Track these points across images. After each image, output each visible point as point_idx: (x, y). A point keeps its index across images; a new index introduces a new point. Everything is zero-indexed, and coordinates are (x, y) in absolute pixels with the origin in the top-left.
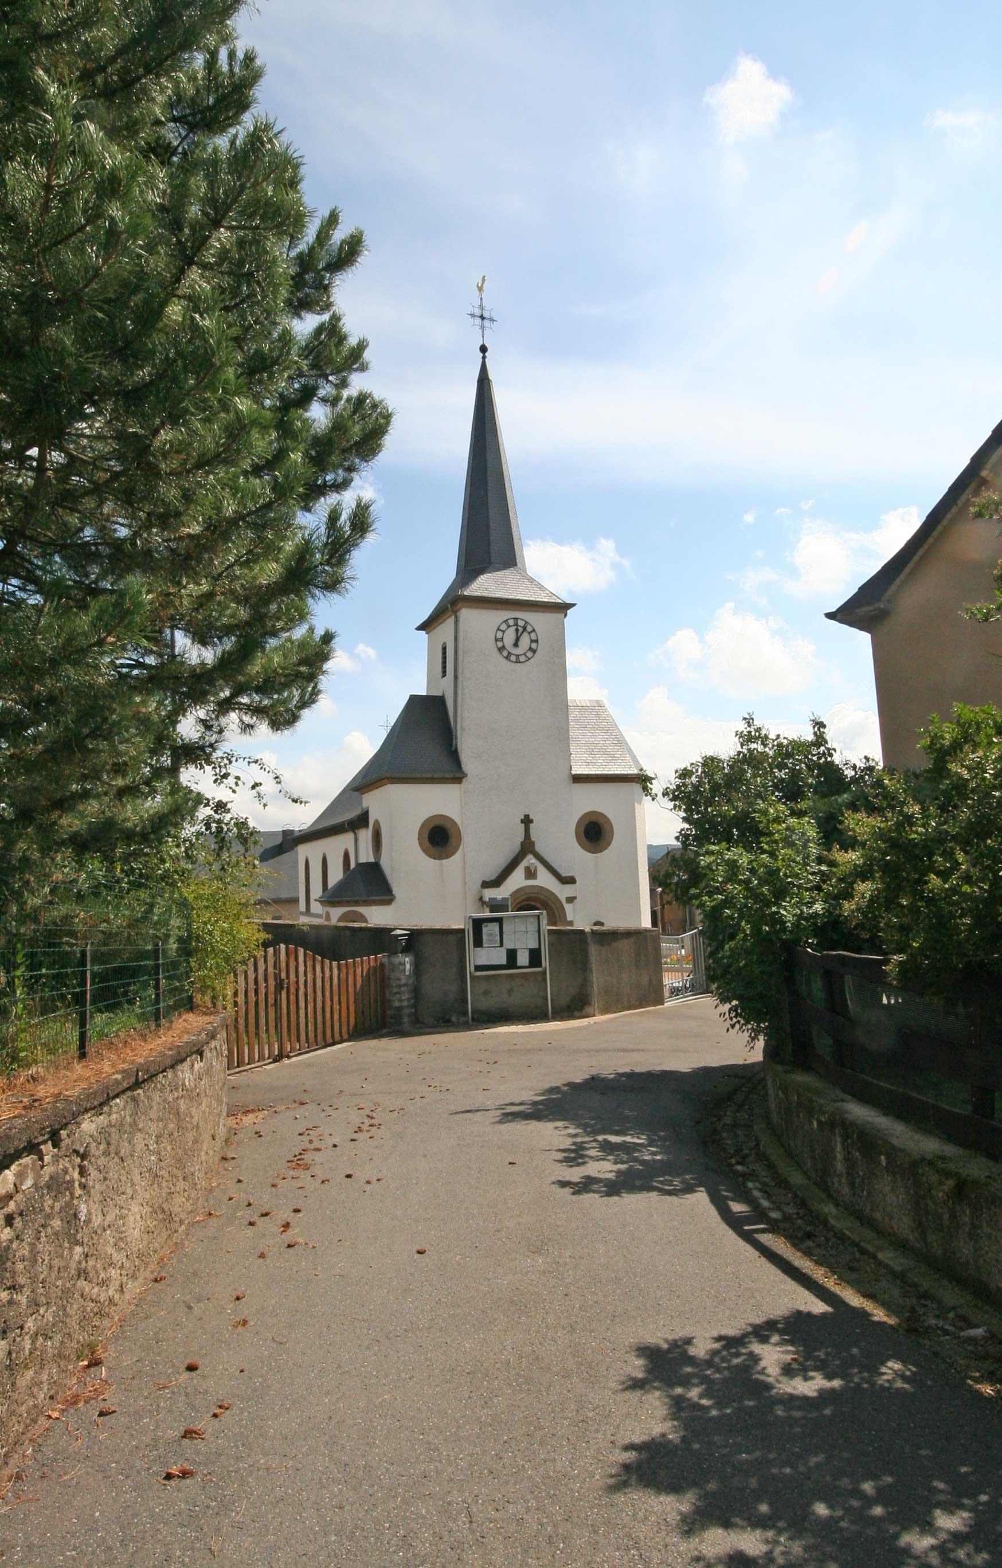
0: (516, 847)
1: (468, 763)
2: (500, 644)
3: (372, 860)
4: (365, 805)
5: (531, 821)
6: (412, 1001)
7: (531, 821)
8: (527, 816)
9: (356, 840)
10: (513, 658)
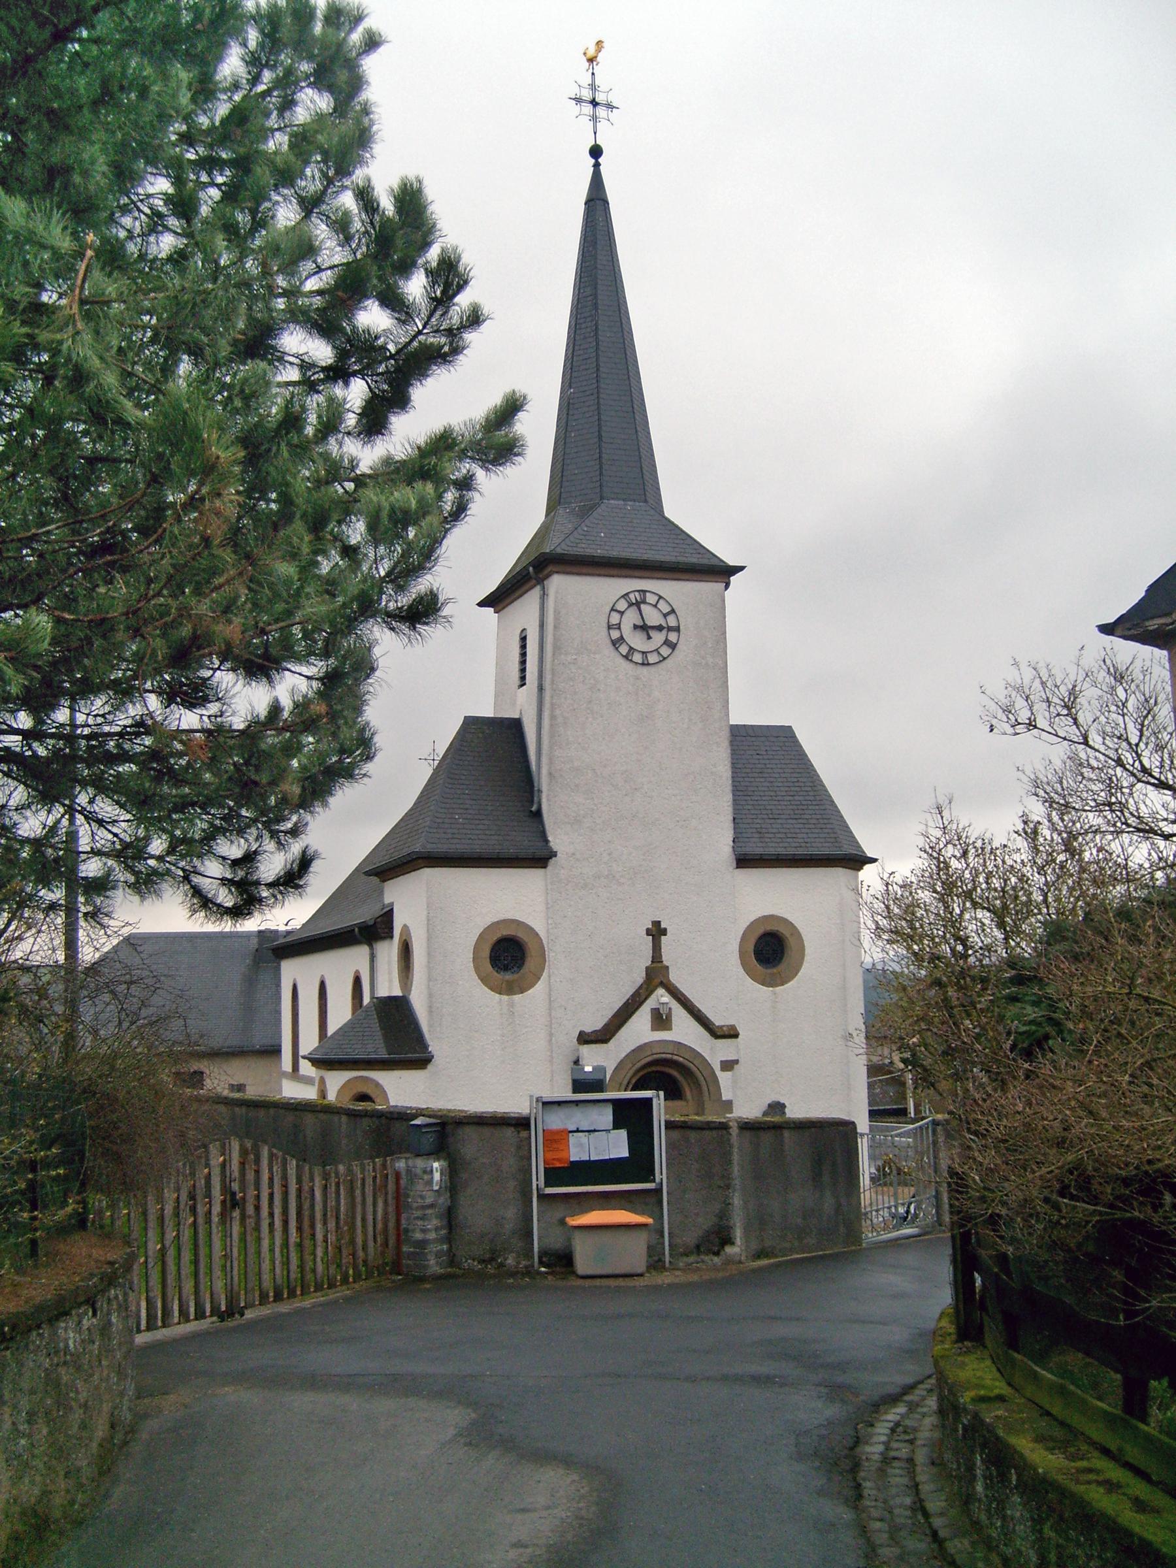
0: (639, 977)
1: (558, 839)
2: (615, 634)
3: (397, 992)
4: (387, 901)
5: (664, 932)
6: (443, 1232)
7: (664, 932)
8: (657, 924)
9: (373, 958)
10: (637, 658)
